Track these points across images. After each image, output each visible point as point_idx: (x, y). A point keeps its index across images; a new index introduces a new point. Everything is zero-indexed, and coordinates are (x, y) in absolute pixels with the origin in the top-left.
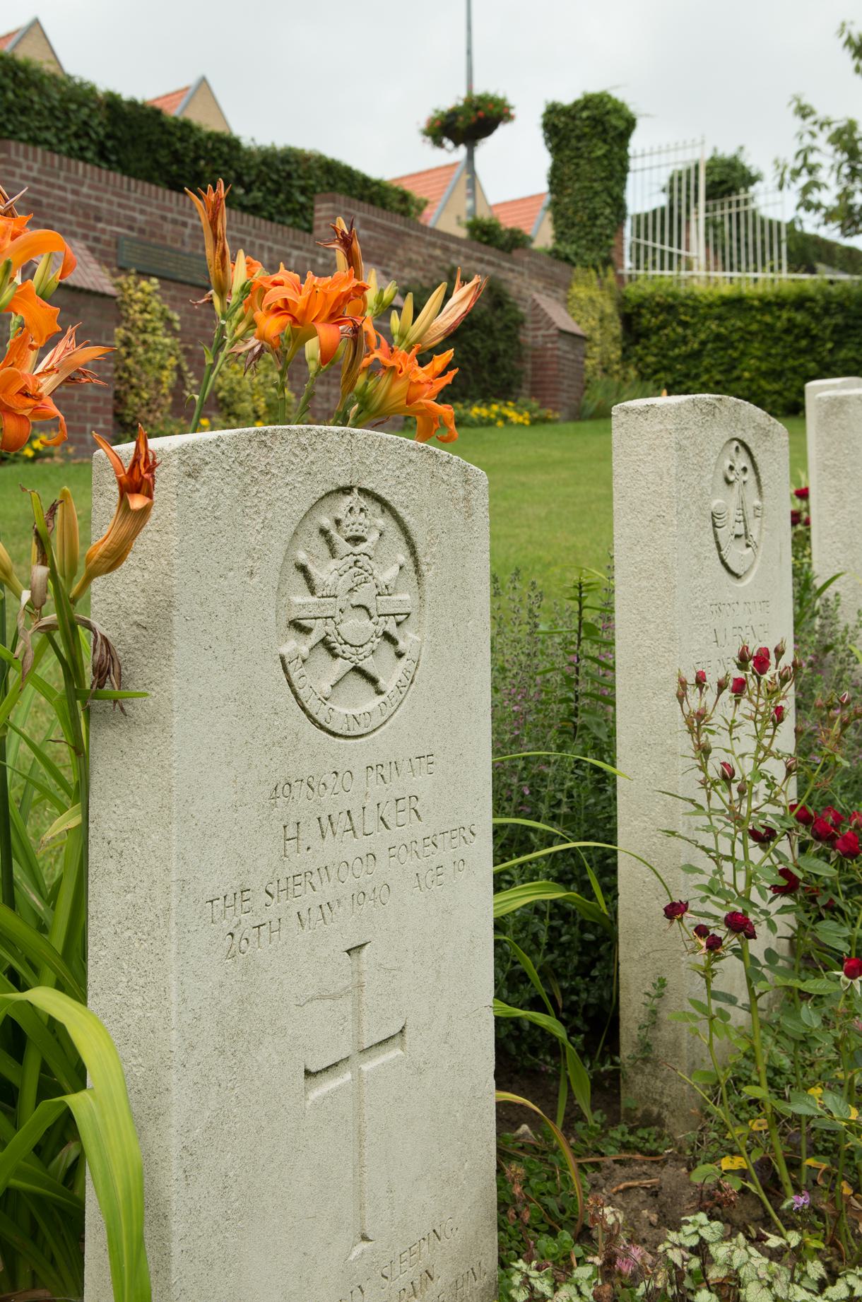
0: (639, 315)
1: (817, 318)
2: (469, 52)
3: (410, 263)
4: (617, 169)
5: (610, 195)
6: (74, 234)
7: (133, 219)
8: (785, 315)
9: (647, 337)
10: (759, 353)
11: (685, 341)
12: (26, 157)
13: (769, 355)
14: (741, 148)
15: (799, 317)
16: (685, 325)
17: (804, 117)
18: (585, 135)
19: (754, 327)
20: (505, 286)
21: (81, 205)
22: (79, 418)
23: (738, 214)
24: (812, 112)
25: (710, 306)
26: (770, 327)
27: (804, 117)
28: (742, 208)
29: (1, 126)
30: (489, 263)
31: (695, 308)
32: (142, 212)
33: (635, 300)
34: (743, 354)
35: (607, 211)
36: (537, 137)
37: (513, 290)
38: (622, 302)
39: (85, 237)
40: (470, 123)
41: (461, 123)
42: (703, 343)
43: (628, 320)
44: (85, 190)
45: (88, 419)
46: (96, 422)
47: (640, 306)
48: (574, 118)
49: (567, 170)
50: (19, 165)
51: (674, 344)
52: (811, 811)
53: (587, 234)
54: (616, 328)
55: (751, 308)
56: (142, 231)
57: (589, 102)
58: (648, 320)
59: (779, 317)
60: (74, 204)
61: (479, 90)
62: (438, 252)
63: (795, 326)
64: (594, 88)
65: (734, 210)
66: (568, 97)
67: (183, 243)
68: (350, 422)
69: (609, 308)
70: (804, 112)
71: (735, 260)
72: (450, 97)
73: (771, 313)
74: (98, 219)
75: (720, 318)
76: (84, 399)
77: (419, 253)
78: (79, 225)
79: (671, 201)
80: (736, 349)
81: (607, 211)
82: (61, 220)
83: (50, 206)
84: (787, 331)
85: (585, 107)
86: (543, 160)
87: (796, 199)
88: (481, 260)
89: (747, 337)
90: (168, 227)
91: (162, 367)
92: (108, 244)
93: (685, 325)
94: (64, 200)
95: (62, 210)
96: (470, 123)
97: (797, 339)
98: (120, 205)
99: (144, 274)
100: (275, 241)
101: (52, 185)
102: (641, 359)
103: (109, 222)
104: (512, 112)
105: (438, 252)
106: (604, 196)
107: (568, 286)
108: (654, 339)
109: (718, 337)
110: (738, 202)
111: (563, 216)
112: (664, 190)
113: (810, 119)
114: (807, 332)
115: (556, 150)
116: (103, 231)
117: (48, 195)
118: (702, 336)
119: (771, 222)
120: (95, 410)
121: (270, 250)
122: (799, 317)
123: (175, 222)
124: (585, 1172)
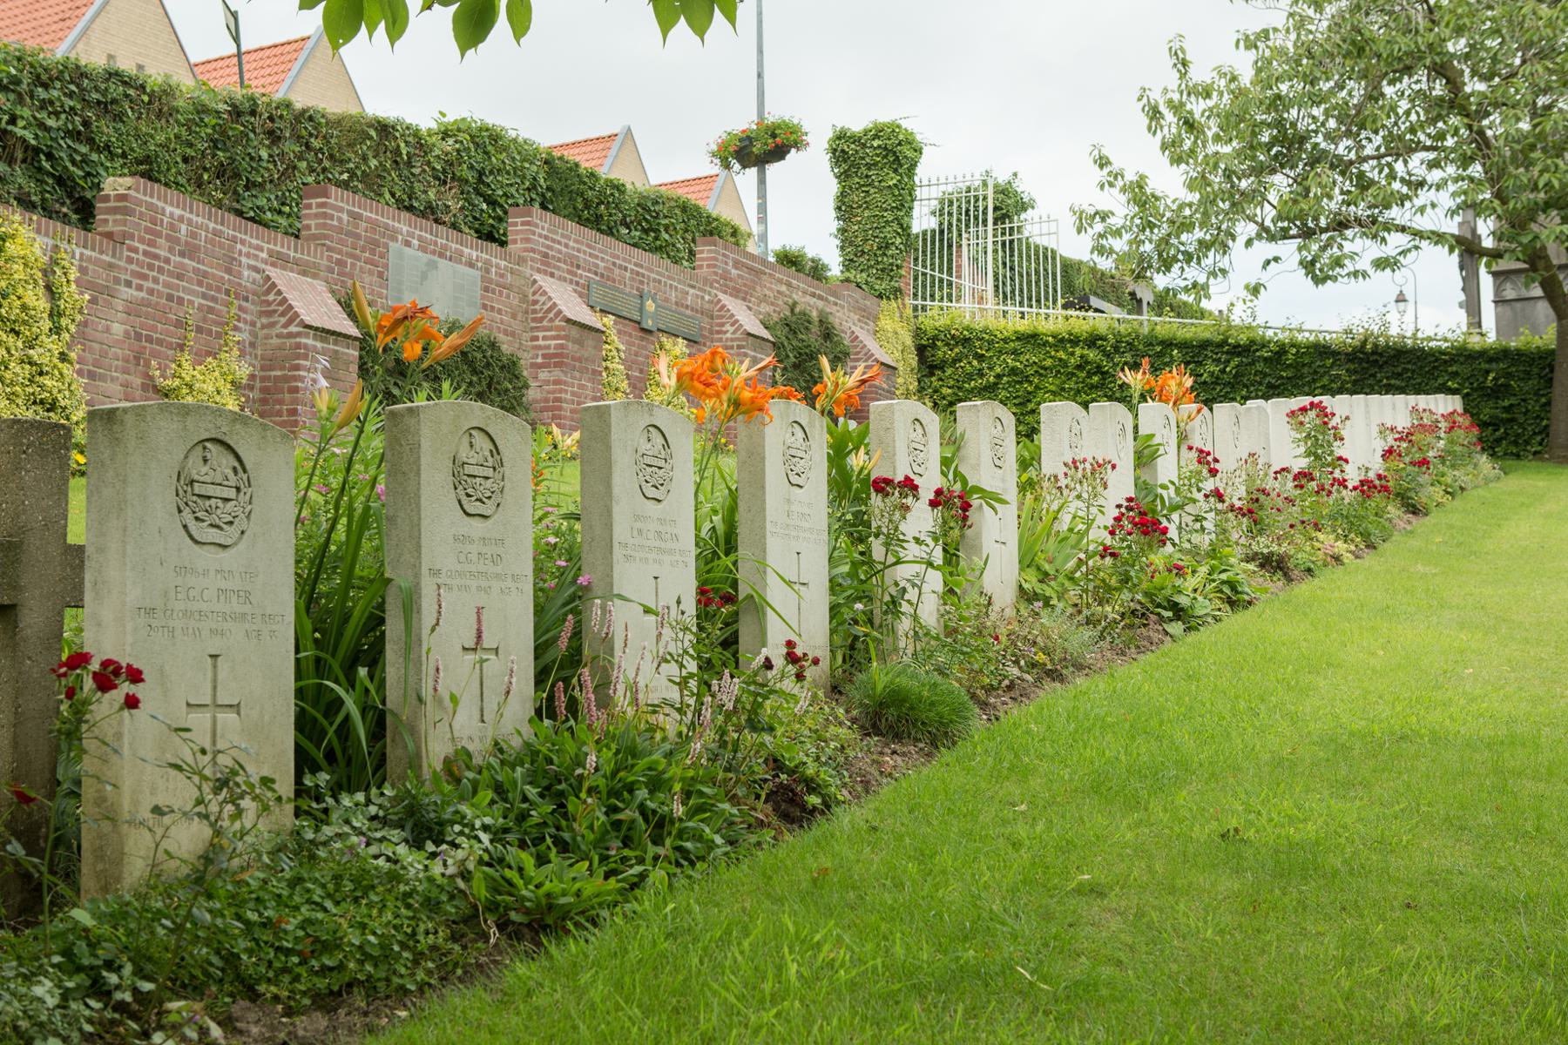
0: (934, 346)
1: (1108, 355)
2: (760, 76)
3: (764, 299)
4: (903, 199)
5: (901, 226)
6: (565, 280)
7: (597, 266)
8: (1078, 351)
9: (942, 369)
10: (1053, 388)
11: (981, 374)
13: (1063, 389)
14: (1015, 175)
15: (1092, 355)
16: (980, 358)
17: (1101, 166)
18: (875, 164)
19: (1048, 362)
20: (831, 319)
23: (1011, 242)
24: (1108, 163)
25: (1005, 341)
26: (1063, 363)
27: (1101, 166)
28: (1015, 236)
30: (820, 298)
31: (990, 342)
33: (930, 333)
34: (1037, 387)
35: (898, 241)
36: (825, 160)
37: (836, 322)
38: (918, 333)
39: (571, 282)
40: (762, 148)
41: (757, 148)
42: (998, 376)
43: (921, 350)
47: (935, 338)
48: (864, 146)
49: (856, 197)
50: (536, 226)
51: (970, 377)
52: (1020, 1000)
53: (878, 263)
54: (913, 360)
55: (1045, 344)
56: (602, 276)
57: (878, 131)
58: (943, 352)
59: (1072, 354)
61: (771, 119)
62: (784, 288)
63: (1088, 363)
64: (884, 117)
65: (1007, 238)
66: (857, 126)
69: (909, 342)
70: (1103, 162)
71: (1009, 289)
72: (742, 120)
73: (1065, 349)
74: (578, 267)
75: (1015, 352)
77: (770, 289)
78: (569, 272)
79: (941, 224)
80: (1031, 383)
81: (898, 241)
84: (1079, 367)
85: (876, 137)
86: (830, 187)
87: (1090, 244)
88: (813, 295)
89: (1042, 371)
90: (617, 271)
93: (980, 358)
94: (560, 252)
95: (559, 260)
96: (762, 148)
97: (1090, 375)
100: (679, 281)
102: (936, 391)
104: (807, 138)
105: (784, 288)
106: (895, 226)
107: (876, 318)
108: (949, 371)
109: (1014, 371)
110: (1011, 229)
111: (851, 244)
112: (933, 213)
113: (1106, 170)
114: (1099, 369)
115: (843, 177)
118: (998, 370)
119: (1037, 247)
122: (1092, 355)
123: (620, 267)
124: (1408, 183)
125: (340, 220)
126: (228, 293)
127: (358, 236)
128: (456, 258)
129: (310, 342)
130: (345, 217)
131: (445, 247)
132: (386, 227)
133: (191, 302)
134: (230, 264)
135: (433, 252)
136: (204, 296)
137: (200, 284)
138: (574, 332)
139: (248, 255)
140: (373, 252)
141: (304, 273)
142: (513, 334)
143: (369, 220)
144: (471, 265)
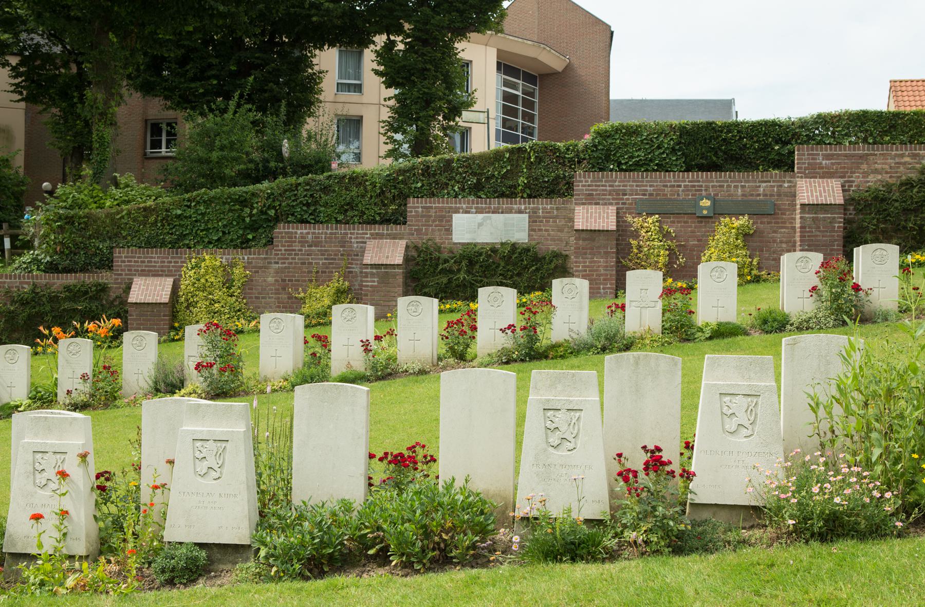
3: (876, 171)
12: (584, 177)
21: (614, 191)
22: (596, 284)
29: (921, 452)
32: (651, 186)
44: (617, 183)
45: (600, 284)
46: (585, 262)
56: (651, 195)
60: (610, 191)
62: (907, 159)
67: (678, 195)
68: (798, 248)
74: (626, 195)
76: (600, 275)
78: (613, 199)
82: (604, 199)
83: (597, 195)
91: (659, 256)
92: (631, 204)
94: (606, 190)
95: (604, 195)
98: (637, 186)
99: (650, 214)
101: (599, 186)
103: (632, 195)
116: (628, 199)
117: (596, 190)
120: (604, 280)
121: (743, 187)
125: (416, 212)
126: (342, 255)
127: (431, 216)
128: (510, 211)
129: (369, 270)
130: (420, 210)
131: (498, 208)
132: (451, 208)
133: (317, 264)
134: (343, 243)
135: (488, 212)
136: (326, 259)
137: (322, 255)
138: (584, 235)
139: (357, 238)
140: (440, 221)
141: (394, 238)
142: (561, 240)
143: (436, 207)
144: (520, 212)
